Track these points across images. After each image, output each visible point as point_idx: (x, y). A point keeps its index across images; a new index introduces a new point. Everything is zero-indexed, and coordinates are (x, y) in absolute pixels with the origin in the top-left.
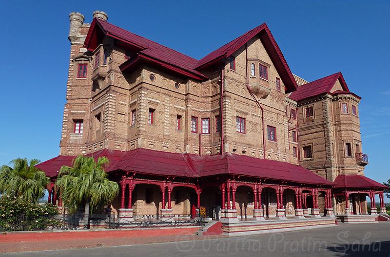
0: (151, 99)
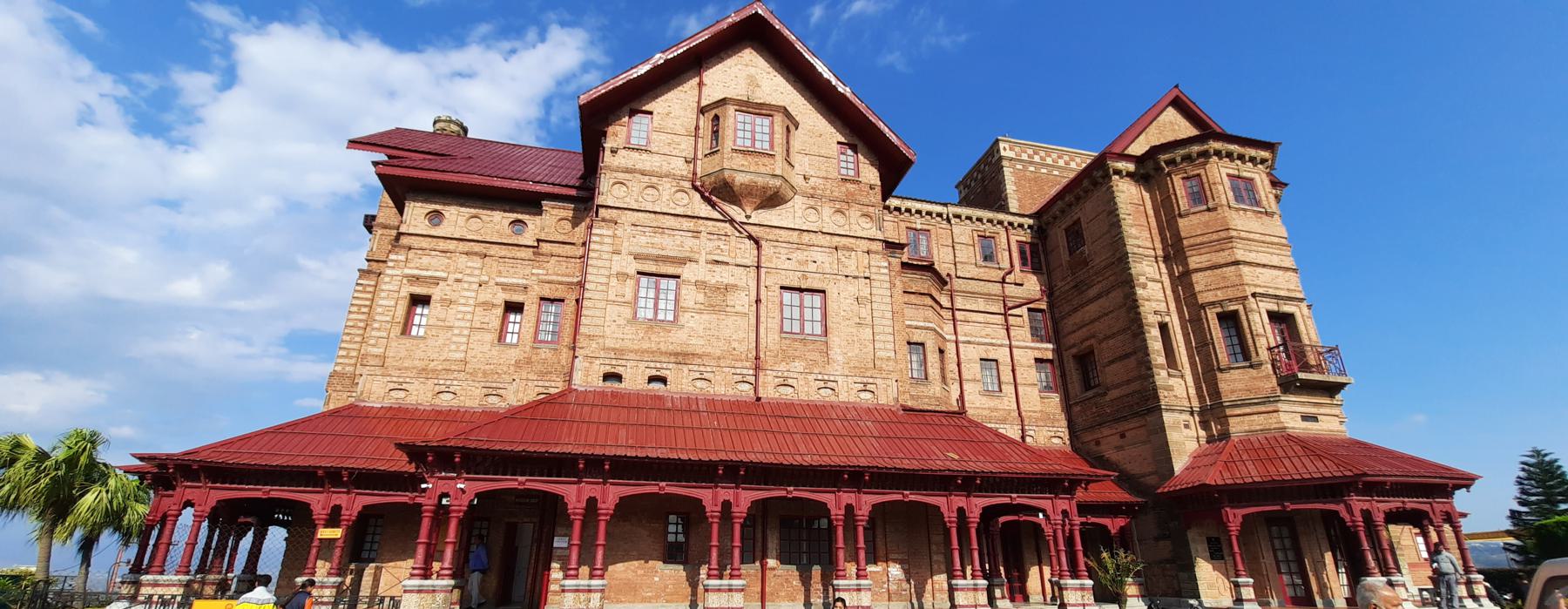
0: (416, 272)
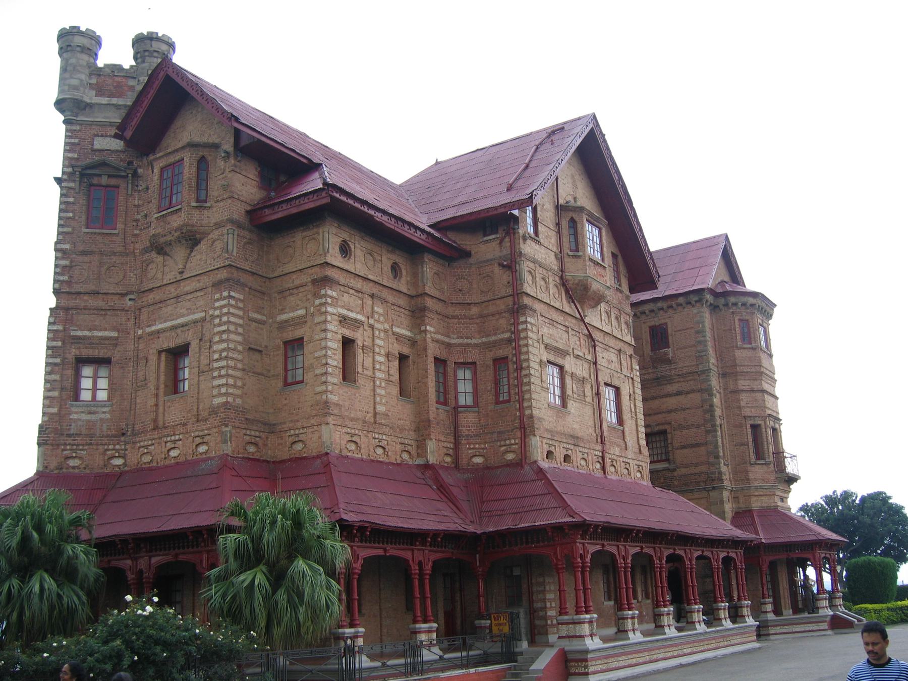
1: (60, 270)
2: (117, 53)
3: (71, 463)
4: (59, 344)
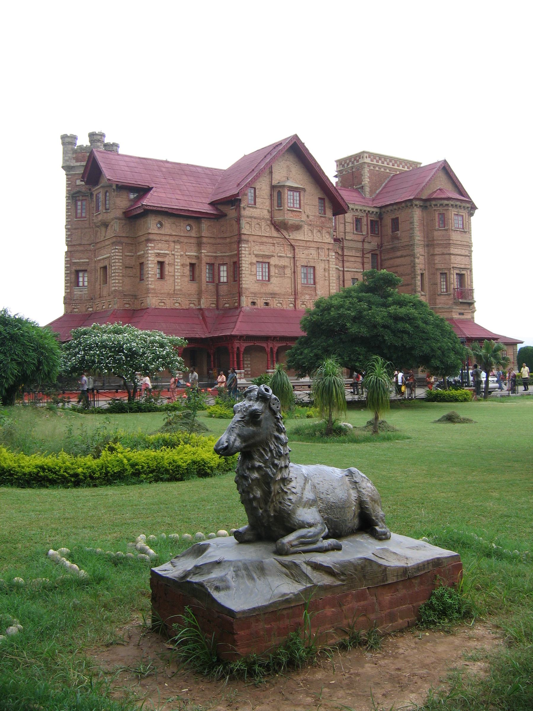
0: (158, 251)
1: (68, 236)
2: (83, 141)
3: (75, 310)
4: (69, 265)
